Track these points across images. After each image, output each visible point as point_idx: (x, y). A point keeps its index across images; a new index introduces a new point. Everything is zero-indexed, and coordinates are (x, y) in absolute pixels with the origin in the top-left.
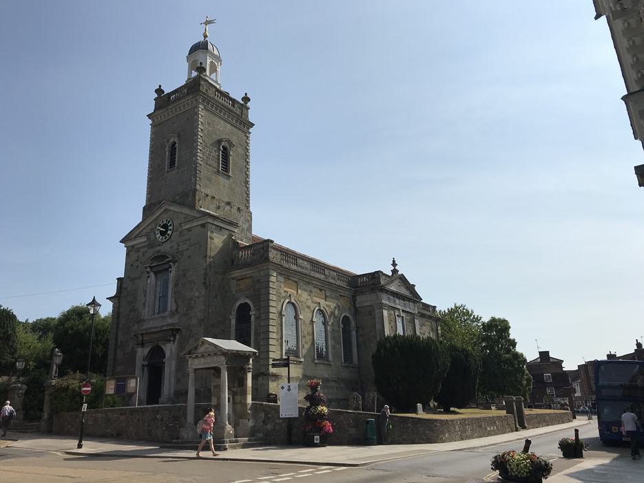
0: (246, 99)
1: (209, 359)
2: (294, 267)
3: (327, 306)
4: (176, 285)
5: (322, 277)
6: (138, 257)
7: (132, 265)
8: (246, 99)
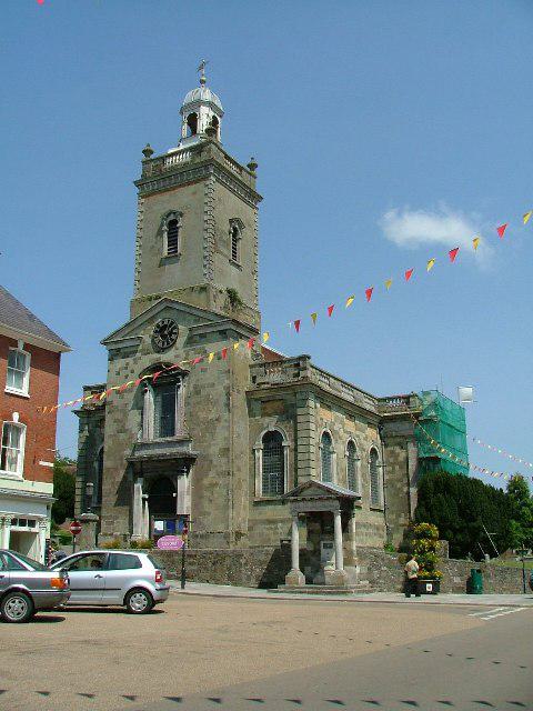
0: (253, 166)
1: (319, 504)
2: (327, 388)
3: (358, 436)
4: (187, 404)
5: (350, 399)
6: (127, 364)
7: (118, 373)
8: (253, 166)
